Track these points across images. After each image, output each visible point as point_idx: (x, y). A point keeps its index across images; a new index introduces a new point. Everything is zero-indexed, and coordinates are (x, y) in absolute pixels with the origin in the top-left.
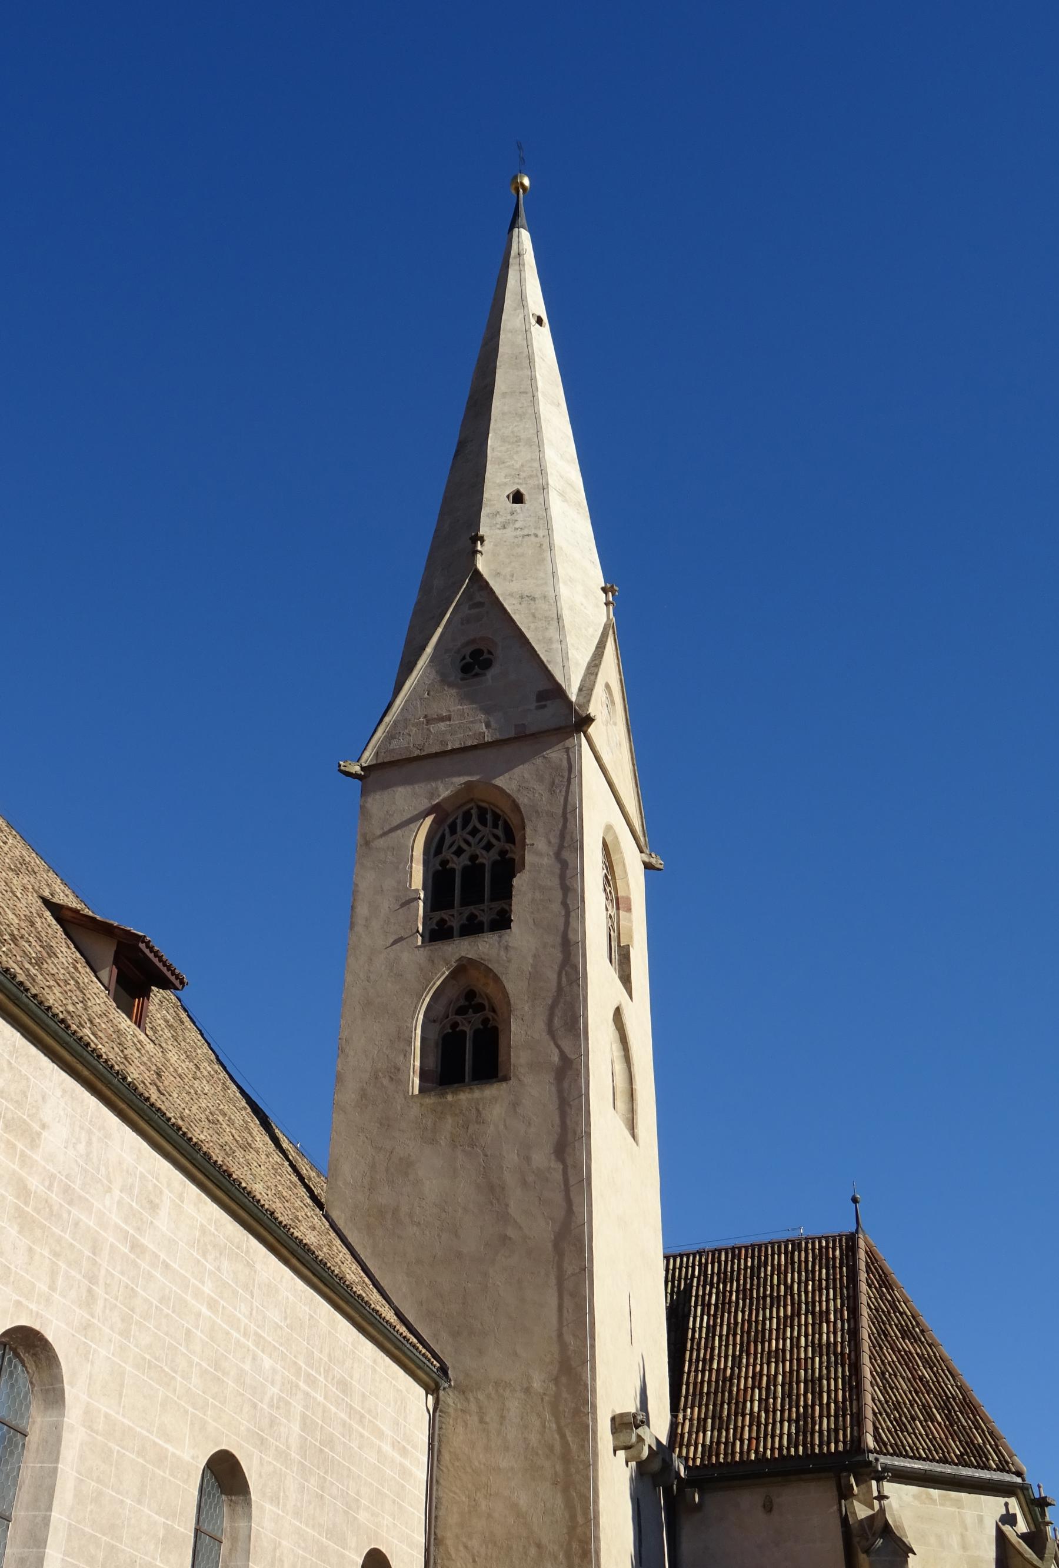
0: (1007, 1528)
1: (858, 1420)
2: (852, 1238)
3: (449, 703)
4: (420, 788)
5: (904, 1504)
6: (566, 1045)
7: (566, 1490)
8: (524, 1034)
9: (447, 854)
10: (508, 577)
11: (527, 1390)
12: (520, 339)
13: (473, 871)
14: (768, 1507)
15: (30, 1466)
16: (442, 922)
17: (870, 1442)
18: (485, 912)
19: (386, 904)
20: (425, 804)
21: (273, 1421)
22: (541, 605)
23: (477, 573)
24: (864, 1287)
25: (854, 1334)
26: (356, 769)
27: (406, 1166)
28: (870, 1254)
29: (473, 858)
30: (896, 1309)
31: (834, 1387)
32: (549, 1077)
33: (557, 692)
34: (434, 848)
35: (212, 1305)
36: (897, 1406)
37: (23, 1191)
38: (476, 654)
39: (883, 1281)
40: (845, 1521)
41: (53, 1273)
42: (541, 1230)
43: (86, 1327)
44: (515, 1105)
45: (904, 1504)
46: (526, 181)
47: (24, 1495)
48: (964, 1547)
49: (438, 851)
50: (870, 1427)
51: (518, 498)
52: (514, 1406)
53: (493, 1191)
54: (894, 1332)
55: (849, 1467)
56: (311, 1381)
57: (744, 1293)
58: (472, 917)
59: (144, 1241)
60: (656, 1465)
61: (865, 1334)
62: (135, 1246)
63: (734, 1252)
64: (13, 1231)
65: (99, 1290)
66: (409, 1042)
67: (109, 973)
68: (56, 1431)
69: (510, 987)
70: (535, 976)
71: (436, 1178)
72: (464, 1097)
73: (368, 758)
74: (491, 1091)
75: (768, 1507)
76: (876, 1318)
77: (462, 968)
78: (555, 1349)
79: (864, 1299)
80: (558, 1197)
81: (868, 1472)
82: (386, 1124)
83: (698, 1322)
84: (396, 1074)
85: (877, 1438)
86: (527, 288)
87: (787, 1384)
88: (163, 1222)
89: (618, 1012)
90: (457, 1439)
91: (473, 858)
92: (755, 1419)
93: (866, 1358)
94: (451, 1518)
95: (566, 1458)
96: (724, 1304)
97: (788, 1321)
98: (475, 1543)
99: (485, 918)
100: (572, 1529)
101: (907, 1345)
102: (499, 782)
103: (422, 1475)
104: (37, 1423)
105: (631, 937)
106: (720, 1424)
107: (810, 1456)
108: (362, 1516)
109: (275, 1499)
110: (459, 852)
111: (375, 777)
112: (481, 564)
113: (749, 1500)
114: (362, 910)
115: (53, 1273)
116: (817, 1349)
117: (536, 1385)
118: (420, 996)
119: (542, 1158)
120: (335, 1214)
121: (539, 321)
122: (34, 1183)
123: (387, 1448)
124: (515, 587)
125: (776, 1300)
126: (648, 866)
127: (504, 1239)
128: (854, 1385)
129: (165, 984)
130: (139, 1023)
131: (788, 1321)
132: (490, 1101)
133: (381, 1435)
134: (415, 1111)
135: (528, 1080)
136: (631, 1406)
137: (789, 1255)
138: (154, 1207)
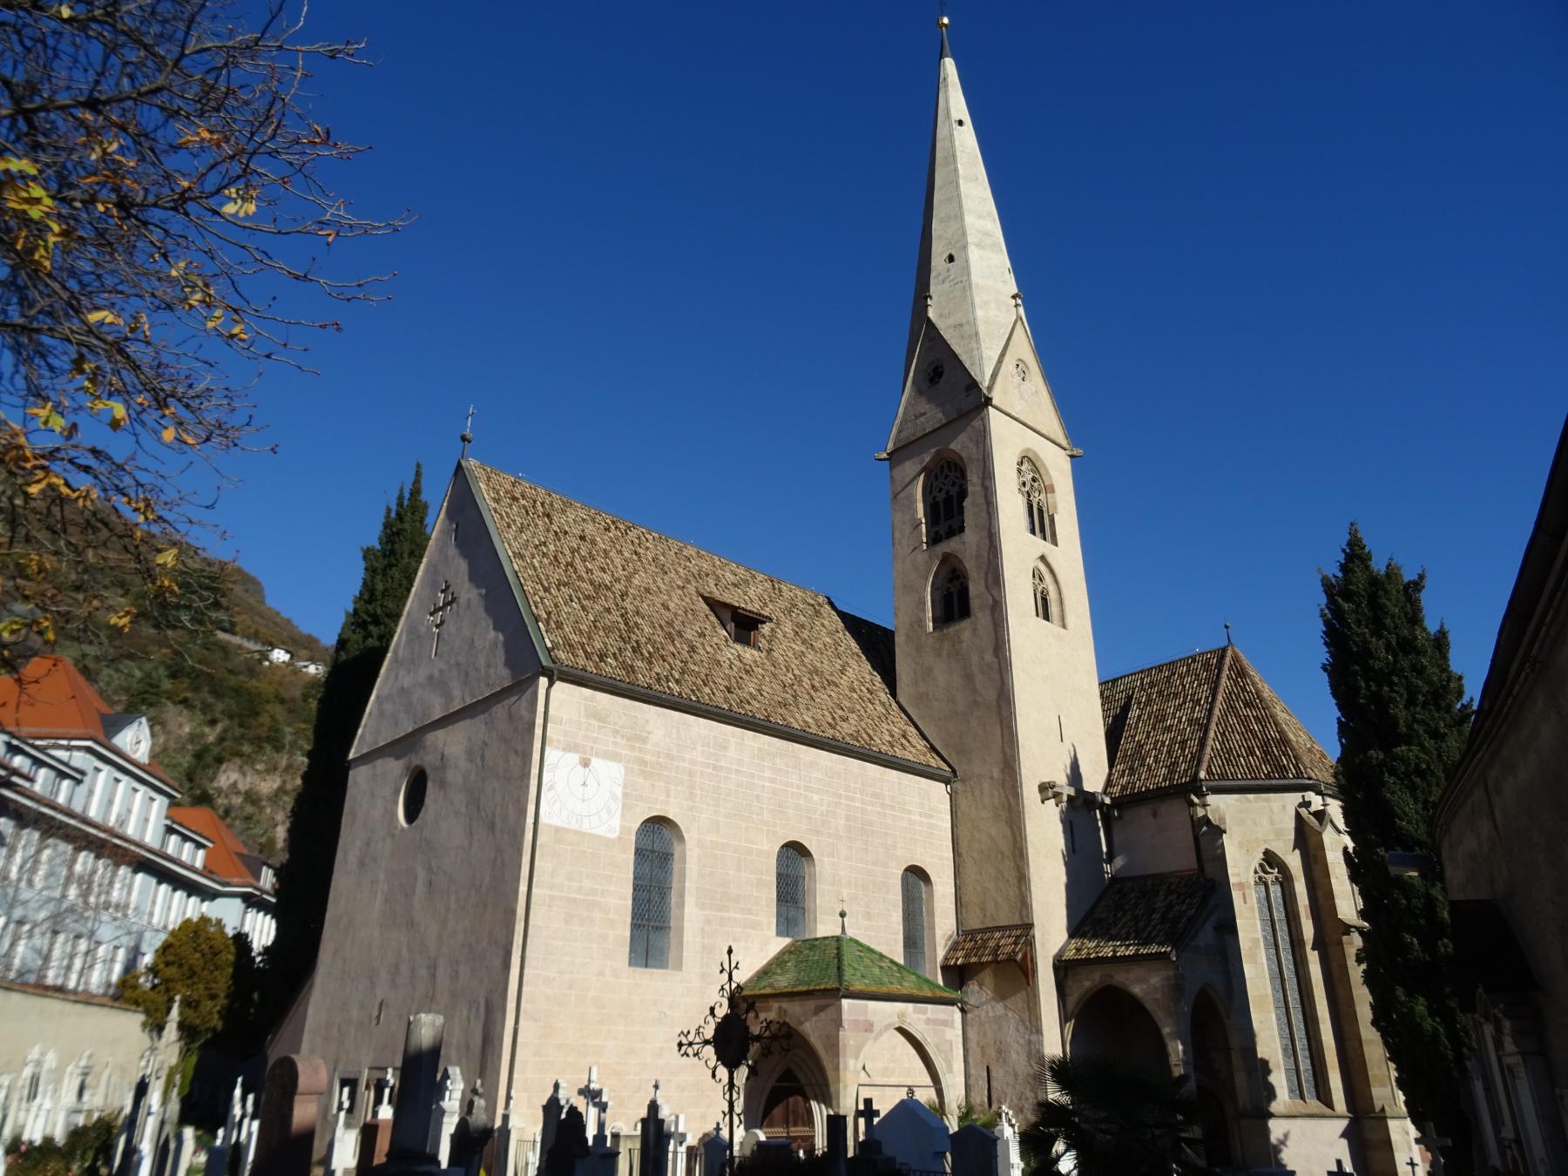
0: (1303, 811)
2: (1224, 650)
3: (924, 406)
4: (916, 460)
5: (1220, 806)
6: (995, 593)
8: (975, 589)
9: (935, 493)
10: (221, 812)
12: (947, 144)
13: (948, 500)
14: (1155, 815)
15: (676, 867)
16: (937, 533)
19: (907, 529)
20: (919, 467)
22: (966, 328)
23: (929, 320)
25: (1210, 711)
27: (928, 672)
30: (1244, 689)
31: (1193, 745)
32: (988, 612)
33: (973, 385)
35: (771, 780)
36: (1229, 751)
37: (643, 762)
38: (936, 369)
39: (1241, 673)
42: (991, 695)
43: (691, 809)
44: (975, 630)
45: (1220, 806)
46: (946, 20)
48: (1272, 823)
50: (1205, 765)
51: (951, 259)
52: (986, 786)
53: (968, 677)
55: (1195, 787)
57: (1160, 693)
59: (722, 764)
61: (1217, 712)
63: (1160, 668)
64: (641, 780)
65: (698, 792)
67: (731, 626)
69: (967, 565)
70: (978, 557)
72: (952, 630)
73: (890, 447)
74: (965, 624)
75: (1155, 815)
76: (1228, 698)
79: (1221, 689)
82: (919, 649)
84: (921, 622)
85: (1209, 771)
86: (954, 101)
87: (1170, 746)
90: (963, 804)
93: (1213, 727)
94: (964, 843)
95: (1010, 809)
96: (1149, 701)
97: (1179, 708)
98: (975, 854)
100: (1015, 841)
102: (952, 446)
104: (677, 850)
105: (1055, 508)
106: (1132, 771)
111: (895, 457)
112: (931, 314)
113: (1145, 811)
114: (897, 535)
116: (1190, 721)
121: (960, 123)
122: (648, 758)
124: (951, 321)
125: (1176, 695)
126: (1072, 457)
127: (976, 702)
128: (1202, 743)
131: (1179, 708)
132: (963, 629)
133: (910, 812)
134: (931, 640)
135: (979, 615)
137: (1189, 665)
138: (724, 748)
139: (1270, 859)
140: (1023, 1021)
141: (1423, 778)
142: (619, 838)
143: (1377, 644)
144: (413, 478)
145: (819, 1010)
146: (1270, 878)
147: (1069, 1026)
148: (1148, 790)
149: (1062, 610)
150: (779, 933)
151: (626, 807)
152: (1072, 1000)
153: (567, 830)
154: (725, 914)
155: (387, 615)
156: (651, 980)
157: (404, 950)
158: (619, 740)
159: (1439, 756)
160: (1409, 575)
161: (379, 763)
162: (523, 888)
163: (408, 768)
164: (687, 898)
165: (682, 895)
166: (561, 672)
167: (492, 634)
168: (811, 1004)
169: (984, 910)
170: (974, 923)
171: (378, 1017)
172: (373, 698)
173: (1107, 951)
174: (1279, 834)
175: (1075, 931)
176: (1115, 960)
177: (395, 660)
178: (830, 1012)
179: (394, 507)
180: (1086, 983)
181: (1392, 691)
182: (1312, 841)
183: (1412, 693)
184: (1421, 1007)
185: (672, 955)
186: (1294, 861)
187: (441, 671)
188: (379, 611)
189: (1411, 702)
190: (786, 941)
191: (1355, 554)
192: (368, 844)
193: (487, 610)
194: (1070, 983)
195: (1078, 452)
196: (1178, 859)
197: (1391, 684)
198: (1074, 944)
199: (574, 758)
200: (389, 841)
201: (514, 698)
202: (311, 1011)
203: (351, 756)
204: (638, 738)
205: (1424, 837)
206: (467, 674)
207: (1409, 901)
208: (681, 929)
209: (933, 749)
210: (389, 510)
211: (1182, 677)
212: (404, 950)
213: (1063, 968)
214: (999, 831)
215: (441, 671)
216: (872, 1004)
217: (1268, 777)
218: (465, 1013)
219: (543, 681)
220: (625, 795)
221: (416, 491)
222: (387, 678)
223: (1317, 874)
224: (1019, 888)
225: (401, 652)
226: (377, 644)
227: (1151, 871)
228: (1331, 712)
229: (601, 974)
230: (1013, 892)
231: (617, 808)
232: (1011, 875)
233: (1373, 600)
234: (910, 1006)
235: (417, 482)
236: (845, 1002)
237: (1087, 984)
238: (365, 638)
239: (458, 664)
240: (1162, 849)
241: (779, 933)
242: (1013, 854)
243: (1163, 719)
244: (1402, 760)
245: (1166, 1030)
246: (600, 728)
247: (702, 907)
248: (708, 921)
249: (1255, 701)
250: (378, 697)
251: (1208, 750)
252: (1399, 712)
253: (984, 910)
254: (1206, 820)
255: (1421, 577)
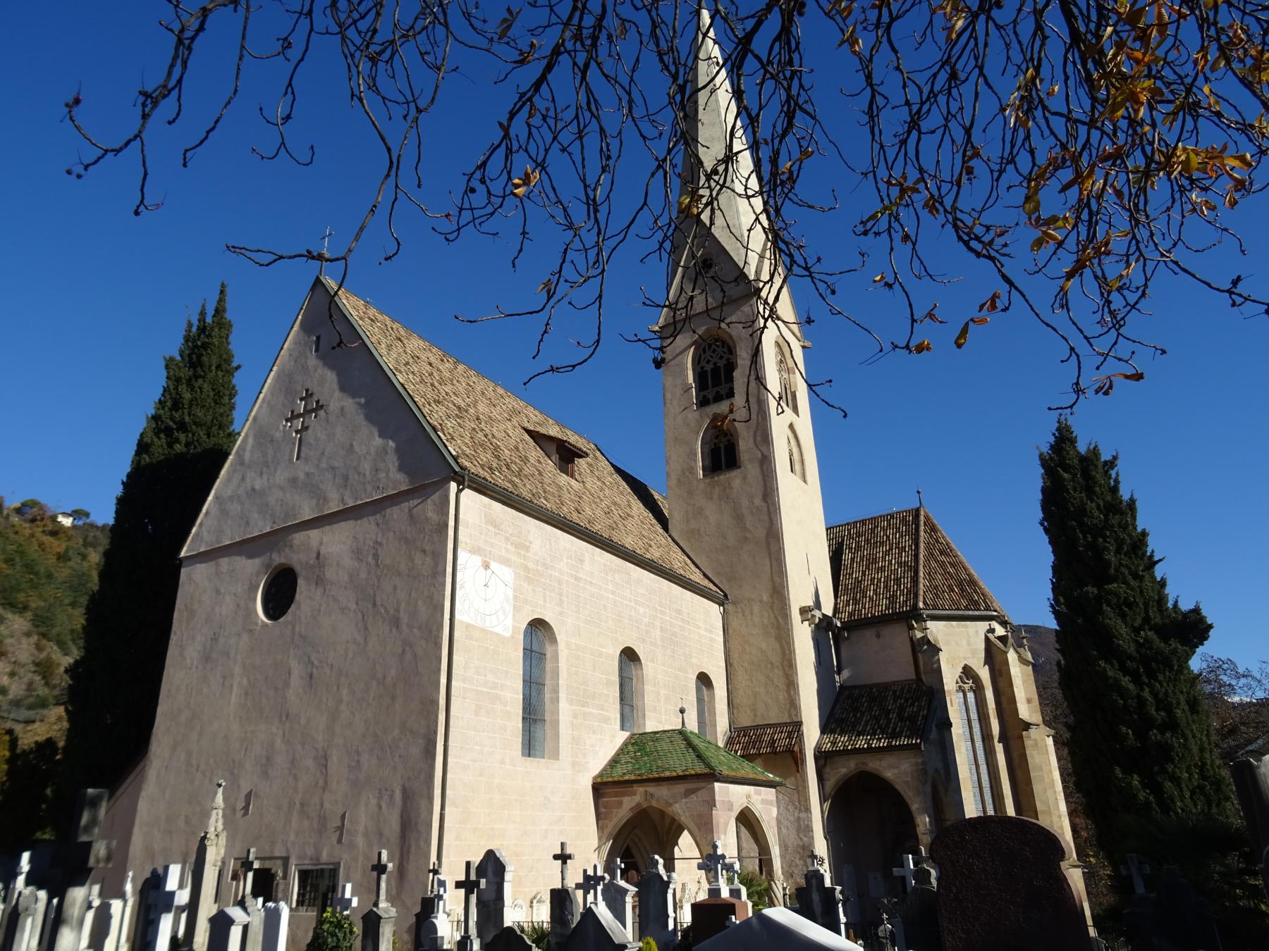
0: (990, 635)
1: (916, 596)
2: (918, 510)
5: (937, 630)
6: (764, 449)
7: (780, 643)
8: (745, 445)
9: (703, 363)
11: (761, 601)
13: (716, 370)
14: (878, 636)
15: (549, 666)
17: (921, 605)
18: (723, 389)
19: (679, 391)
20: (689, 341)
21: (647, 632)
24: (922, 533)
25: (916, 556)
26: (657, 328)
27: (700, 511)
28: (927, 517)
29: (715, 364)
30: (937, 541)
31: (907, 582)
32: (757, 464)
34: (697, 361)
35: (613, 593)
37: (527, 569)
39: (933, 529)
40: (911, 639)
41: (545, 597)
42: (760, 533)
43: (561, 613)
44: (744, 479)
45: (937, 630)
47: (548, 676)
49: (699, 362)
50: (921, 598)
53: (738, 518)
54: (937, 553)
55: (913, 616)
56: (663, 613)
57: (867, 541)
58: (717, 392)
59: (580, 575)
60: (824, 624)
61: (921, 556)
62: (576, 578)
63: (863, 522)
65: (565, 599)
66: (696, 455)
67: (555, 457)
68: (556, 651)
71: (714, 514)
72: (722, 477)
75: (878, 636)
76: (928, 548)
77: (715, 418)
78: (538, 734)
79: (922, 539)
80: (766, 518)
81: (920, 619)
82: (690, 493)
83: (847, 556)
84: (692, 470)
85: (925, 603)
88: (587, 566)
89: (791, 426)
90: (734, 623)
91: (715, 364)
92: (871, 599)
93: (921, 567)
94: (735, 655)
95: (778, 627)
96: (858, 547)
97: (887, 553)
98: (746, 665)
99: (723, 392)
101: (943, 558)
103: (722, 640)
104: (549, 650)
106: (856, 602)
107: (894, 614)
108: (694, 661)
109: (652, 661)
110: (708, 362)
113: (869, 634)
114: (668, 396)
115: (545, 597)
116: (900, 564)
117: (765, 599)
118: (698, 434)
119: (758, 501)
120: (674, 535)
122: (530, 565)
123: (702, 632)
125: (882, 543)
126: (803, 347)
127: (746, 538)
128: (915, 581)
129: (581, 457)
130: (572, 476)
131: (887, 553)
133: (699, 627)
134: (702, 486)
135: (749, 467)
136: (810, 602)
137: (889, 521)
138: (582, 561)
139: (968, 672)
140: (792, 802)
141: (1130, 609)
142: (512, 637)
143: (1091, 506)
144: (217, 297)
145: (688, 793)
146: (967, 687)
147: (827, 805)
148: (874, 616)
149: (803, 469)
150: (622, 729)
151: (516, 609)
152: (830, 784)
153: (474, 627)
154: (587, 710)
155: (195, 423)
156: (533, 764)
157: (278, 742)
158: (509, 547)
159: (1141, 592)
160: (1105, 456)
161: (224, 562)
162: (443, 681)
163: (268, 566)
164: (561, 695)
165: (556, 691)
166: (471, 480)
167: (378, 441)
168: (681, 788)
169: (754, 710)
170: (745, 721)
171: (246, 808)
172: (210, 498)
173: (861, 743)
174: (974, 652)
175: (824, 729)
176: (870, 750)
177: (240, 460)
178: (702, 794)
179: (195, 323)
180: (844, 769)
181: (1105, 541)
182: (998, 658)
183: (1120, 544)
184: (1136, 781)
185: (548, 745)
186: (984, 674)
187: (307, 474)
188: (187, 419)
189: (1118, 552)
190: (626, 734)
191: (1064, 438)
192: (215, 639)
193: (369, 418)
194: (827, 770)
195: (808, 344)
196: (898, 669)
197: (1104, 537)
198: (826, 739)
199: (477, 560)
200: (245, 637)
201: (416, 502)
202: (143, 806)
203: (183, 554)
204: (523, 547)
205: (1134, 654)
206: (346, 478)
207: (1125, 701)
208: (556, 723)
209: (705, 575)
210: (190, 325)
211: (884, 529)
212: (278, 742)
213: (820, 756)
214: (769, 646)
215: (307, 474)
216: (731, 786)
217: (967, 609)
218: (373, 801)
219: (453, 486)
220: (515, 597)
221: (219, 311)
222: (229, 479)
223: (1001, 685)
224: (788, 692)
225: (247, 456)
226: (185, 450)
227: (877, 679)
228: (1043, 556)
229: (503, 762)
230: (782, 696)
231: (509, 608)
232: (780, 681)
233: (1086, 474)
234: (752, 788)
235: (221, 300)
236: (717, 785)
237: (844, 771)
238: (170, 445)
239: (333, 468)
240: (885, 662)
241: (622, 729)
242: (782, 664)
243: (875, 561)
244: (1115, 594)
245: (914, 807)
246: (496, 534)
247: (571, 704)
248: (575, 716)
249: (946, 551)
250: (216, 497)
251: (921, 586)
252: (1111, 557)
253: (754, 710)
254: (925, 640)
255: (1115, 458)
